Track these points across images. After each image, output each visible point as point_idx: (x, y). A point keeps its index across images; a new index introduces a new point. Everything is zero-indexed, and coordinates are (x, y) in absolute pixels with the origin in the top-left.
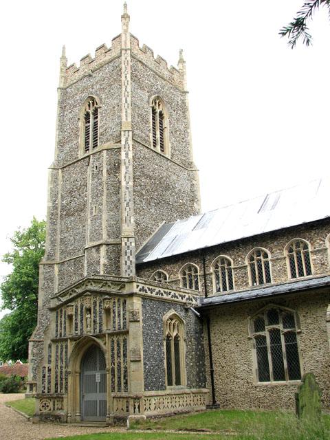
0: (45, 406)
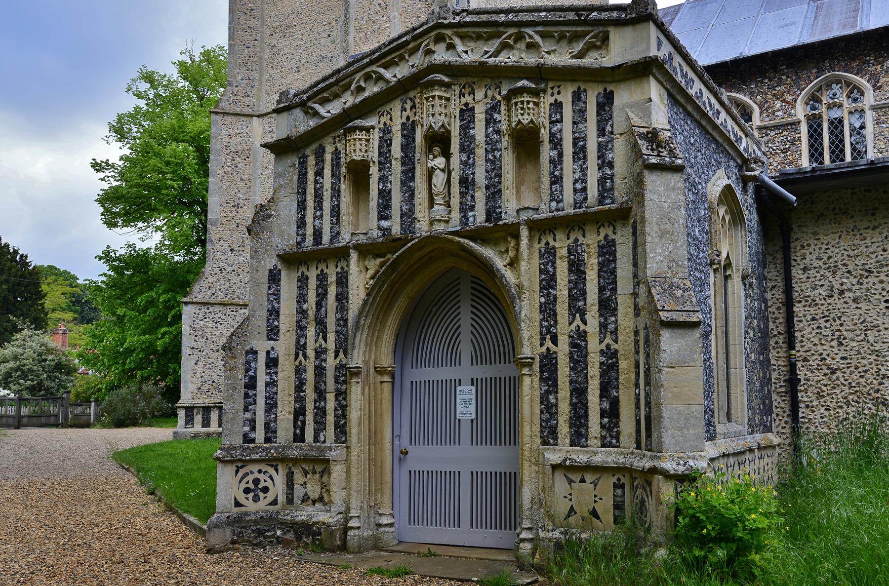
0: (256, 490)
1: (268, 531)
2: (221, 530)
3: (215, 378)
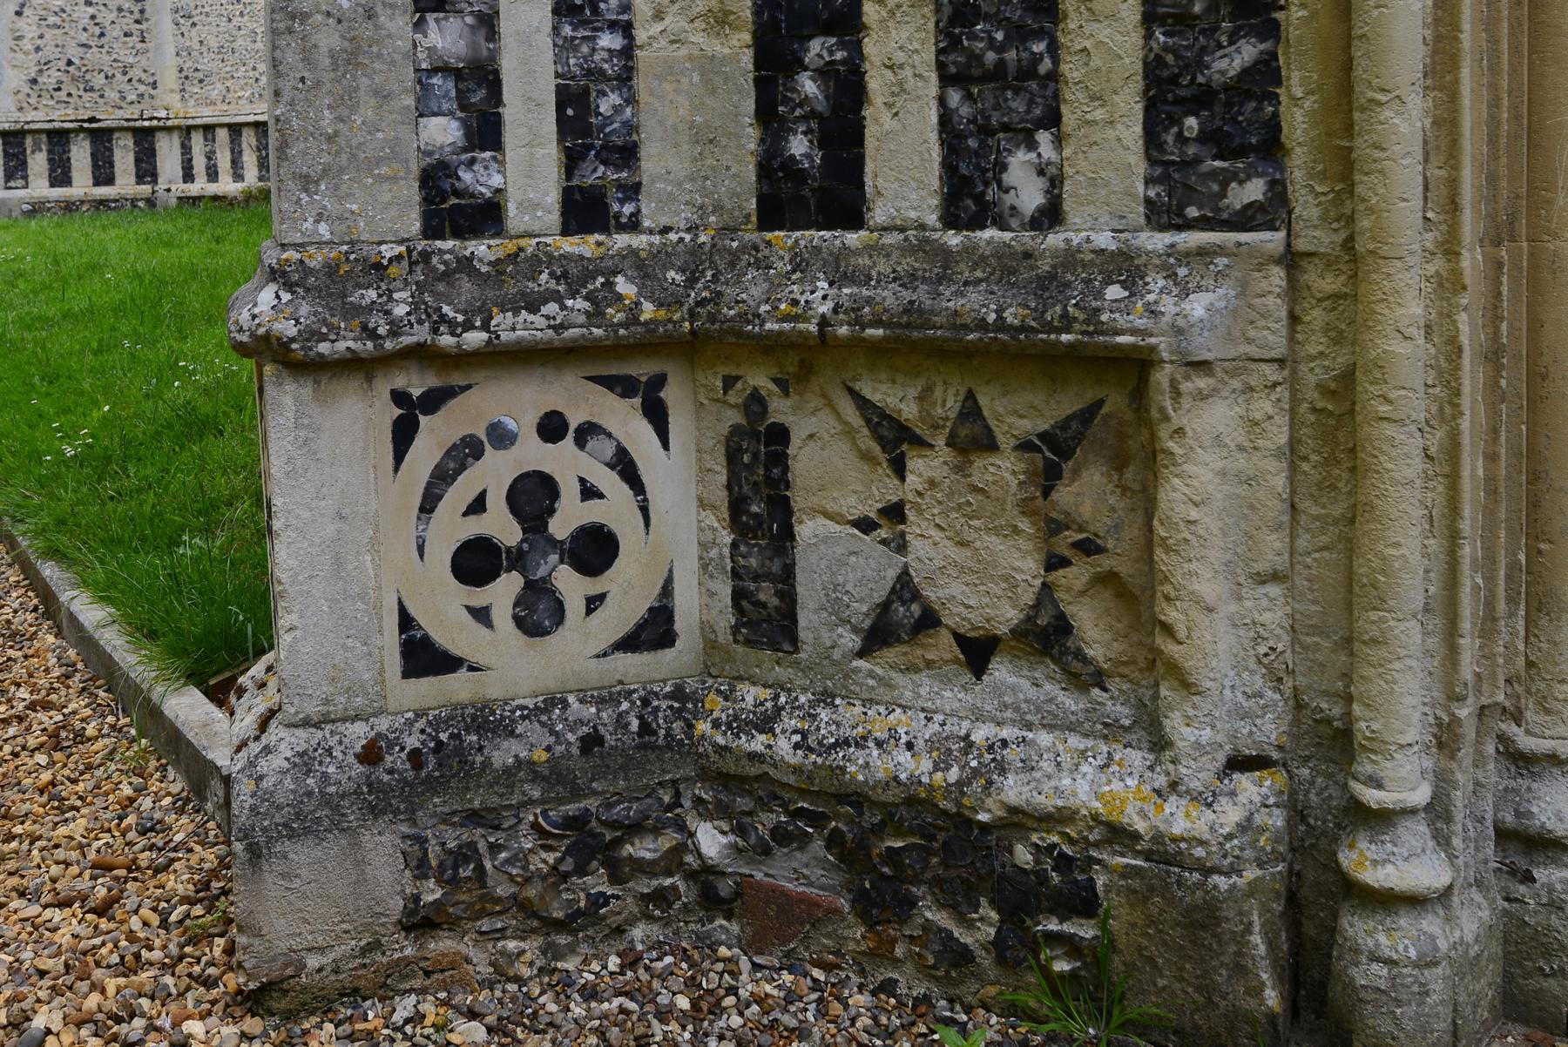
0: (532, 553)
1: (634, 829)
2: (335, 845)
3: (73, 52)
